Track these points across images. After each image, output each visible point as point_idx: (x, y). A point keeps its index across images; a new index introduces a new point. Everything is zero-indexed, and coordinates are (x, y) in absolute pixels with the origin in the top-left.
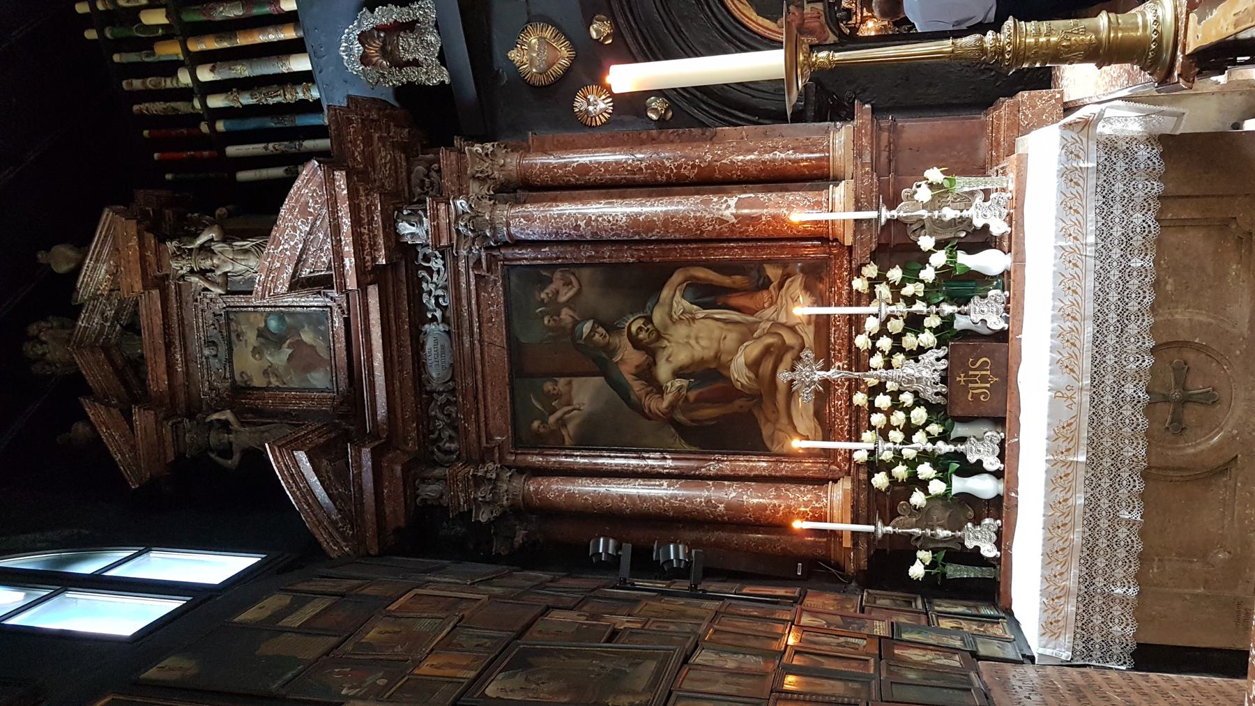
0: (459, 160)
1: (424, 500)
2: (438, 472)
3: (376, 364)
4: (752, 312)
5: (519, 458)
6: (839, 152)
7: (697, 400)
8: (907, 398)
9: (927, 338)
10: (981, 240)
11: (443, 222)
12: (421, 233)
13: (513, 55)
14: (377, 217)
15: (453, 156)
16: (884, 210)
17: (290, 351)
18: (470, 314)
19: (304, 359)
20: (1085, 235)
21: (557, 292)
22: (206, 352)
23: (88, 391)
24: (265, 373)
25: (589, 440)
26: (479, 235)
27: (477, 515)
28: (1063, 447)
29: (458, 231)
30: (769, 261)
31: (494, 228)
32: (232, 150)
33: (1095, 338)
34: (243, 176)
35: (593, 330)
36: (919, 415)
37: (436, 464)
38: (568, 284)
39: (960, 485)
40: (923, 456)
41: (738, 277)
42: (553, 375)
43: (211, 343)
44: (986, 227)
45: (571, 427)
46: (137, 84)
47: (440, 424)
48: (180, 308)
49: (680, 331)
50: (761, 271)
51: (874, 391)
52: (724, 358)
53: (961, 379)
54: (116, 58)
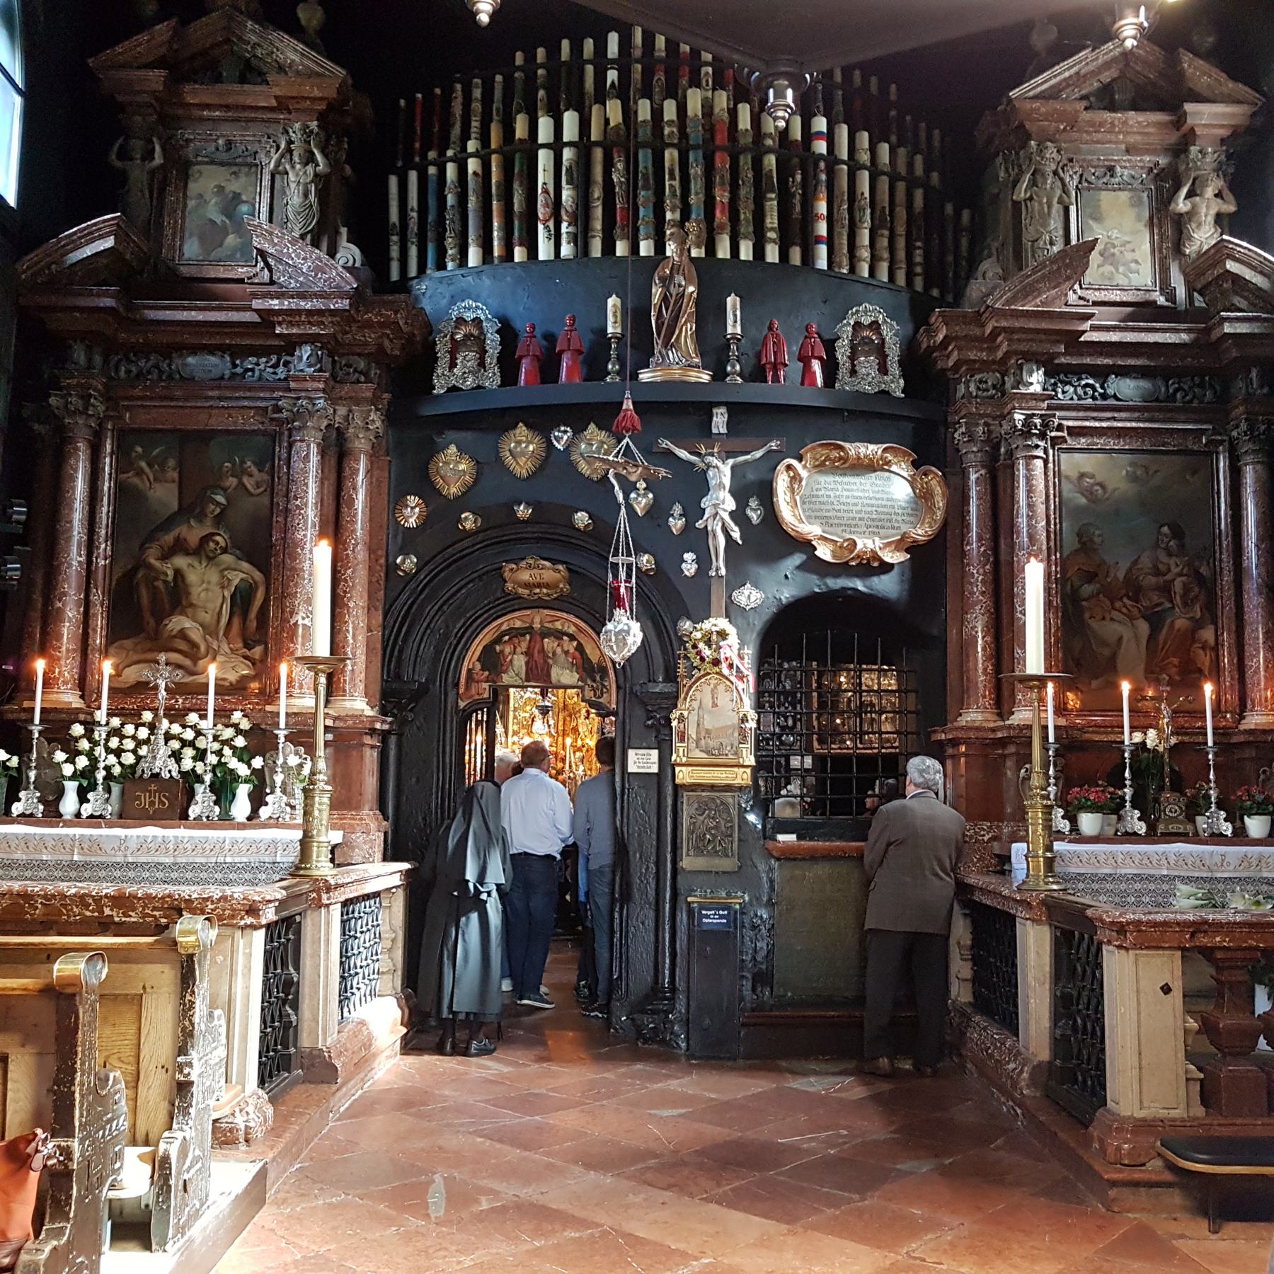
0: (365, 400)
1: (70, 347)
2: (98, 359)
3: (193, 313)
4: (226, 634)
5: (109, 434)
6: (348, 704)
7: (155, 587)
8: (143, 751)
9: (187, 764)
10: (257, 800)
11: (309, 385)
12: (301, 366)
13: (453, 449)
14: (315, 330)
15: (369, 394)
16: (285, 732)
17: (218, 221)
18: (237, 399)
19: (213, 235)
20: (232, 856)
21: (251, 476)
22: (221, 142)
23: (184, 22)
24: (201, 196)
25: (123, 493)
26: (296, 416)
27: (56, 395)
28: (85, 846)
29: (298, 398)
30: (266, 648)
31: (300, 428)
32: (413, 176)
33: (161, 864)
34: (393, 181)
35: (218, 504)
36: (129, 759)
37: (106, 361)
38: (258, 485)
39: (71, 787)
40: (94, 761)
41: (255, 624)
42: (181, 466)
43: (229, 145)
44: (266, 804)
45: (136, 480)
46: (477, 93)
47: (142, 363)
48: (263, 120)
49: (214, 576)
50: (258, 642)
51: (152, 727)
52: (189, 611)
53: (153, 787)
54: (499, 78)
